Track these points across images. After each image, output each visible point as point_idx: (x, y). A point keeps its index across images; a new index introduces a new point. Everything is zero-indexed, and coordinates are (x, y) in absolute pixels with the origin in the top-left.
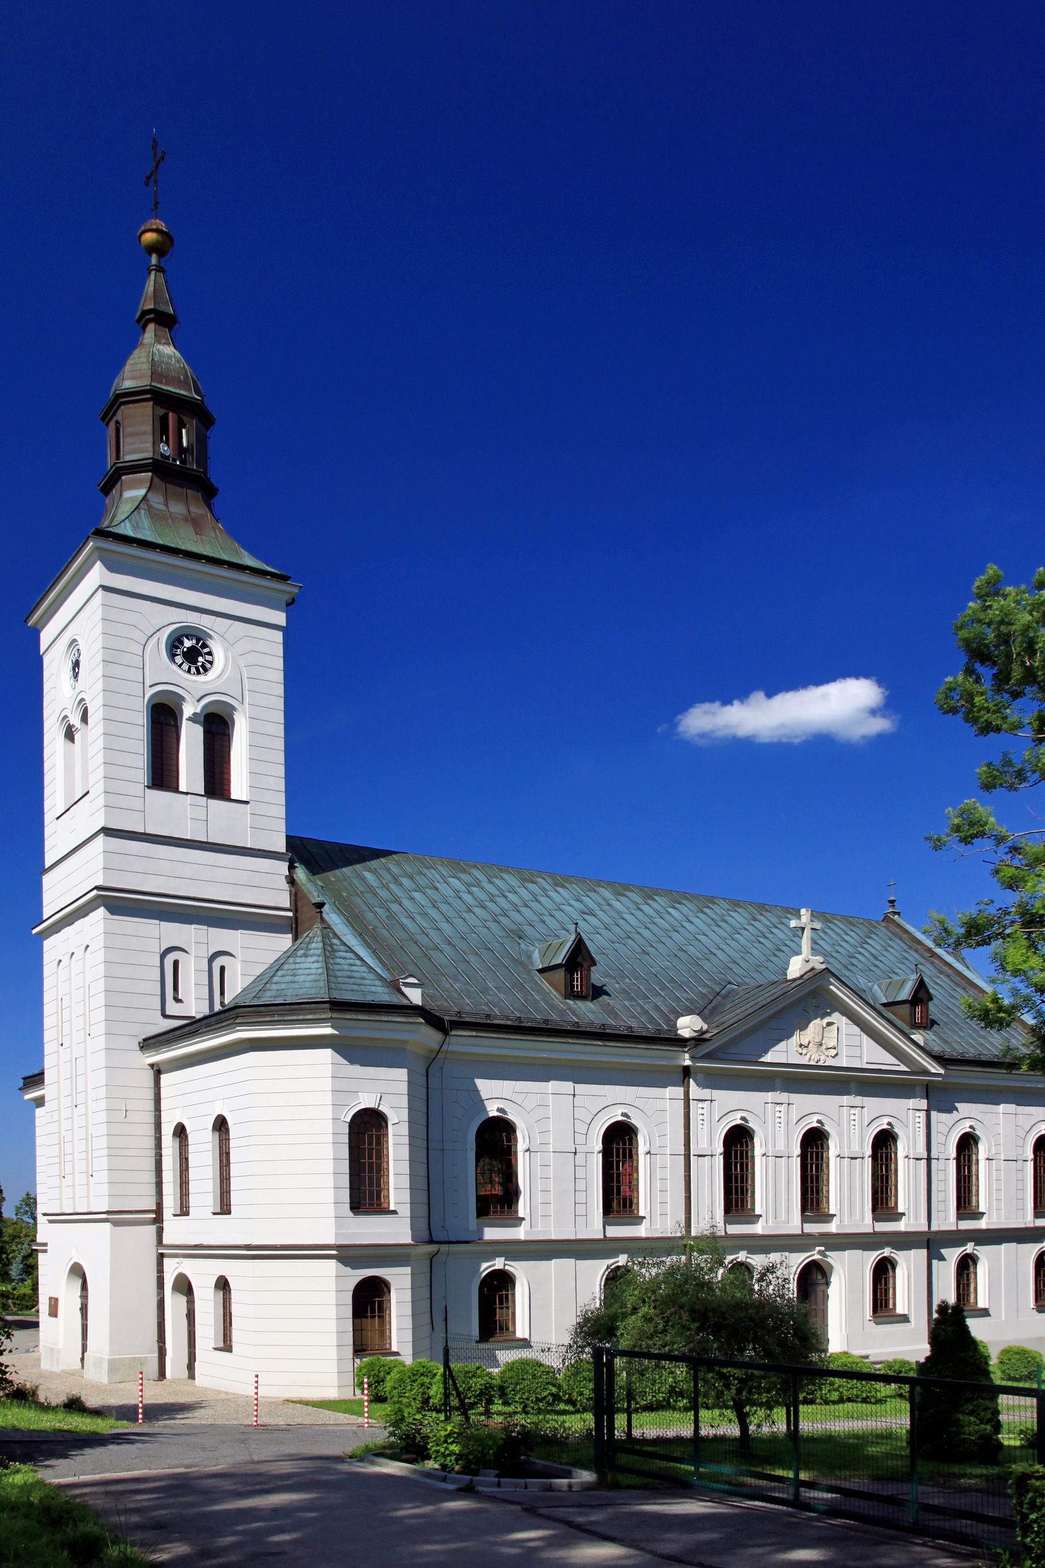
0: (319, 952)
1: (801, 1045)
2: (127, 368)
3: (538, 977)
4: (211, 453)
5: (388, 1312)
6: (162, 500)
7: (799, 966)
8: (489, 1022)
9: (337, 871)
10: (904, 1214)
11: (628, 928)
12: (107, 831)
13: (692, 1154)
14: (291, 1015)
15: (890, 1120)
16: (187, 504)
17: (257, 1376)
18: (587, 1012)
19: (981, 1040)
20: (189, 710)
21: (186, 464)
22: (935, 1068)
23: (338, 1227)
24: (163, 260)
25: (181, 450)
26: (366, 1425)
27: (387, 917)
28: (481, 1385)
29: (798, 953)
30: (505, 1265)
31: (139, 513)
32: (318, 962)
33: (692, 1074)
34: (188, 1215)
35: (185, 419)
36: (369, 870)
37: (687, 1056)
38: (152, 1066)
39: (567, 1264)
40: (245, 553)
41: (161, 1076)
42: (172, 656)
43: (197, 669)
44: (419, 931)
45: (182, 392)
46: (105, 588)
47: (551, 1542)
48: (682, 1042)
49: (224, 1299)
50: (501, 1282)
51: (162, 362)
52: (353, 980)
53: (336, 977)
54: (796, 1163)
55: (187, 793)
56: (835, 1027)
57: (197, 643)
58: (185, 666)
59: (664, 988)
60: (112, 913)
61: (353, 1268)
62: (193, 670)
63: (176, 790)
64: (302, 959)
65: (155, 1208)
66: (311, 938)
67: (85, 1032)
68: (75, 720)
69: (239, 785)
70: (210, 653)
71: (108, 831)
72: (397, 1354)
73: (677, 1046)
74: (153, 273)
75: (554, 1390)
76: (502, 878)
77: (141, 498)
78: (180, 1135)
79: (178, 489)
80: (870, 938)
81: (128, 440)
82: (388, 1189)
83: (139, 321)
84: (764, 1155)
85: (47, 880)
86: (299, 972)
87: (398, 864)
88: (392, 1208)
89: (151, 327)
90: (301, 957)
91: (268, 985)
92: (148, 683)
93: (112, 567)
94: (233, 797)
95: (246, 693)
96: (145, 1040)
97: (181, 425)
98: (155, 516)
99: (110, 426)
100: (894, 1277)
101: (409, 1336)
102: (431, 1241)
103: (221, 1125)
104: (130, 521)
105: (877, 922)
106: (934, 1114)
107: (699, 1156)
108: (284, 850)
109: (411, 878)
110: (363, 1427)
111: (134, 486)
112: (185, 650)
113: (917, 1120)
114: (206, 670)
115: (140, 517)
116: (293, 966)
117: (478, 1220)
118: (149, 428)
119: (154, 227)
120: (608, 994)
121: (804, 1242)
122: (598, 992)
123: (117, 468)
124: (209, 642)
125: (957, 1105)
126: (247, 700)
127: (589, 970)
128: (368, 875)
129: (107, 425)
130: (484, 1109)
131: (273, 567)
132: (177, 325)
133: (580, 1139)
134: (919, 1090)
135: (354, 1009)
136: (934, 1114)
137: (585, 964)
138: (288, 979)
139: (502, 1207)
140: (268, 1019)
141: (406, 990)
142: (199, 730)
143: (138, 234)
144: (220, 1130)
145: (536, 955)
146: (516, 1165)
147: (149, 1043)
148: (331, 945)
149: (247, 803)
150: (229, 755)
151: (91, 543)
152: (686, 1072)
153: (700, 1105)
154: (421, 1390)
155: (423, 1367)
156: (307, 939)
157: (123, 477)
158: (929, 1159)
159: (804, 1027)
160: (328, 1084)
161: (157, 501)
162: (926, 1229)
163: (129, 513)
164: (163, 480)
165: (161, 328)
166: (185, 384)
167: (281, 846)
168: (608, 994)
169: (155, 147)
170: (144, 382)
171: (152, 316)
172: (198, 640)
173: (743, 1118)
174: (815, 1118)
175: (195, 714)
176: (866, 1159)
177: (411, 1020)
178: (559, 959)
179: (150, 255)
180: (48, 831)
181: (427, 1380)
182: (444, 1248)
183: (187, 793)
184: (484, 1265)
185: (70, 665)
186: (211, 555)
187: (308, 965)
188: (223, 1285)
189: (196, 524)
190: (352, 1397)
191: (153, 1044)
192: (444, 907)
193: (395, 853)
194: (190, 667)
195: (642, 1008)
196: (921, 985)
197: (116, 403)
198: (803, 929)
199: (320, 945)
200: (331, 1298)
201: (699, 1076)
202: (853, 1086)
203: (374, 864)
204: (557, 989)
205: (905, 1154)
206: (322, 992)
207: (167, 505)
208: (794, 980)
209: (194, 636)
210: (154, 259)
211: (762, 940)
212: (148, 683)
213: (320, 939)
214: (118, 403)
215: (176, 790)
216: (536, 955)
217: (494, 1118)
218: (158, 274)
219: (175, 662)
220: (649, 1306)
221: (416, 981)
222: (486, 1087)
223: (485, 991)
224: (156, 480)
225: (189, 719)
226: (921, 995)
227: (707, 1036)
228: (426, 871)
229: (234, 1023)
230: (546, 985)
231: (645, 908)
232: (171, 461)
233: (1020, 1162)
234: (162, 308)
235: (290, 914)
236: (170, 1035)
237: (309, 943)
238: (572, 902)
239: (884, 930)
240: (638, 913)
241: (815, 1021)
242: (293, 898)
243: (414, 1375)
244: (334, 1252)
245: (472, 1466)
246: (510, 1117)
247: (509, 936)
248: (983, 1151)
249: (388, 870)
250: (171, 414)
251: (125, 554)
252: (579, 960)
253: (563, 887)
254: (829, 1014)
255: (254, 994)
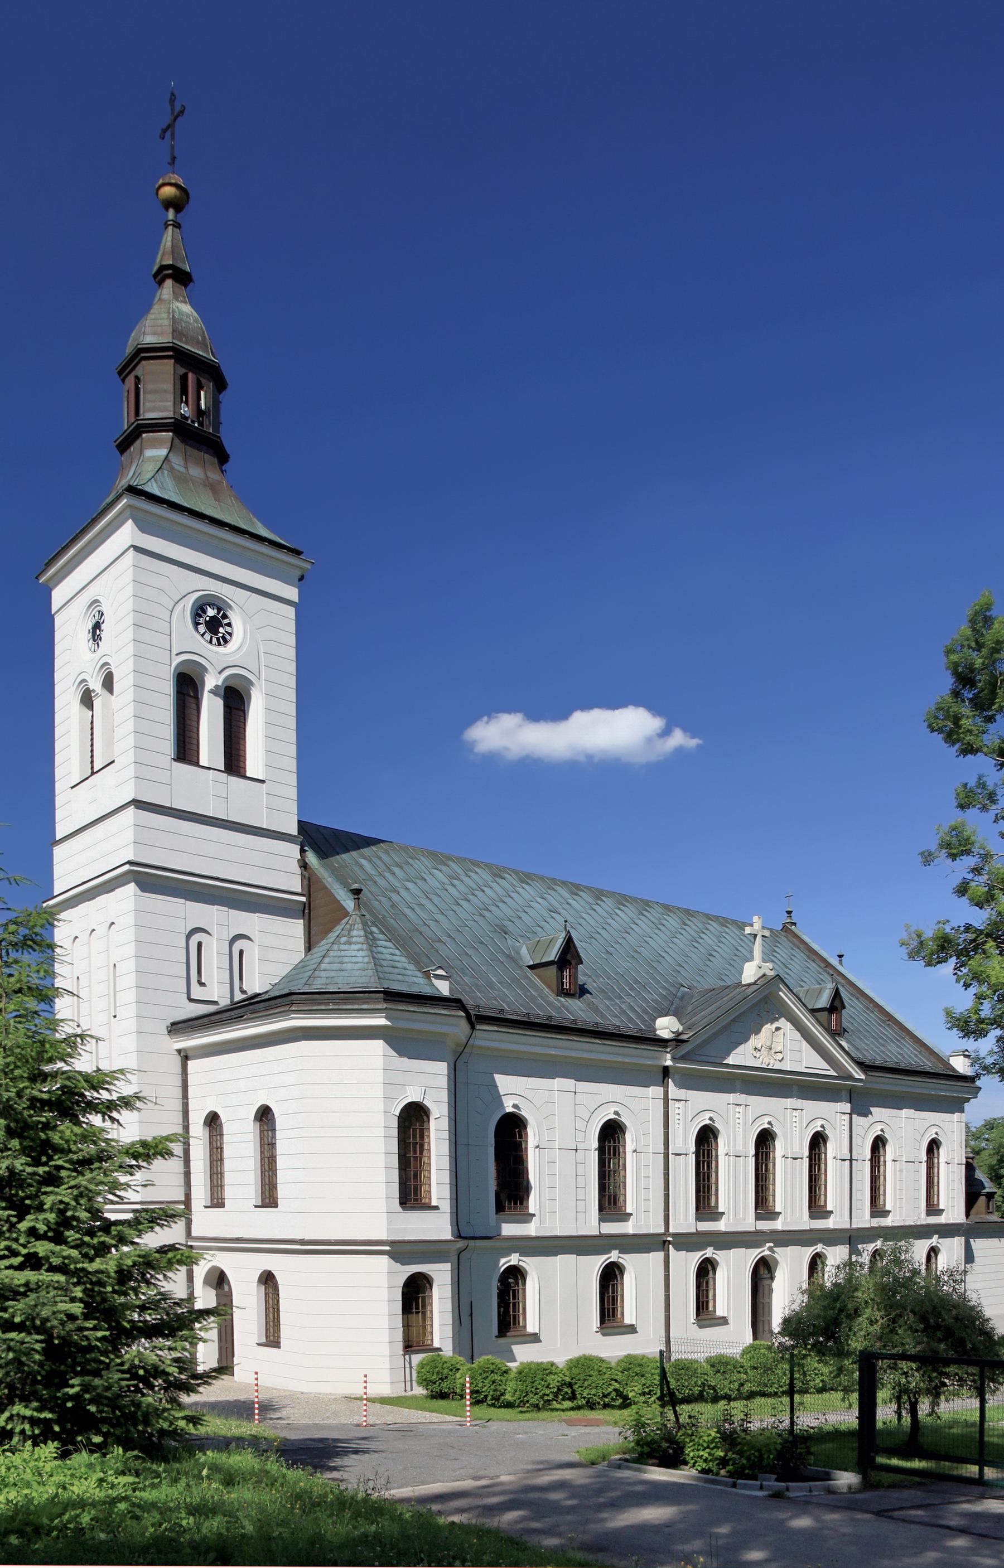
0: (361, 940)
1: (756, 1049)
2: (148, 323)
3: (529, 973)
4: (222, 419)
5: (429, 1308)
6: (182, 463)
7: (753, 972)
8: (502, 1016)
9: (337, 857)
10: (832, 1212)
11: (589, 928)
12: (138, 804)
13: (670, 1152)
14: (345, 1004)
15: (712, 1115)
16: (204, 468)
17: (366, 1376)
18: (575, 1010)
19: (882, 1048)
20: (211, 681)
21: (203, 427)
22: (858, 1074)
23: (390, 1222)
24: (179, 215)
25: (200, 413)
26: (468, 1424)
27: (391, 906)
28: (558, 1381)
29: (751, 959)
30: (519, 1260)
31: (163, 473)
32: (362, 950)
33: (671, 1075)
34: (224, 1207)
35: (203, 380)
36: (365, 858)
37: (669, 1056)
38: (179, 1051)
39: (571, 1258)
40: (260, 524)
41: (189, 1062)
42: (196, 624)
43: (218, 639)
44: (421, 923)
45: (200, 353)
46: (137, 549)
47: (973, 1551)
48: (663, 1042)
49: (266, 1294)
50: (516, 1274)
51: (182, 320)
52: (396, 971)
53: (382, 966)
54: (752, 1161)
55: (209, 768)
56: (781, 1032)
57: (218, 613)
58: (208, 636)
59: (632, 989)
60: (143, 890)
61: (403, 1264)
62: (214, 640)
63: (196, 764)
64: (346, 947)
65: (183, 1199)
66: (351, 926)
67: (110, 1013)
68: (96, 684)
69: (254, 762)
70: (229, 625)
71: (138, 804)
72: (439, 1349)
73: (660, 1046)
74: (170, 228)
75: (617, 1385)
76: (476, 873)
77: (163, 458)
78: (210, 1125)
79: (196, 452)
80: (776, 946)
81: (149, 397)
82: (430, 1185)
83: (155, 276)
84: (727, 1155)
85: (59, 852)
86: (346, 959)
87: (386, 852)
88: (434, 1203)
89: (169, 283)
90: (344, 944)
91: (317, 972)
92: (174, 652)
93: (144, 527)
94: (248, 775)
95: (263, 668)
96: (173, 1024)
97: (199, 387)
98: (180, 480)
99: (127, 381)
100: (524, 1290)
101: (449, 1332)
102: (460, 1237)
103: (265, 1115)
104: (155, 480)
105: (777, 931)
106: (854, 1116)
107: (677, 1155)
108: (296, 834)
109: (401, 867)
110: (466, 1425)
111: (154, 445)
112: (208, 619)
113: (737, 1115)
114: (226, 641)
115: (164, 477)
116: (338, 954)
117: (498, 1216)
118: (169, 386)
119: (173, 181)
120: (591, 994)
121: (758, 1238)
122: (583, 991)
123: (138, 424)
124: (229, 613)
125: (872, 1109)
126: (263, 676)
127: (577, 968)
128: (364, 862)
129: (123, 381)
130: (501, 1104)
131: (281, 539)
132: (192, 284)
133: (580, 1136)
134: (845, 1094)
135: (404, 999)
136: (854, 1116)
137: (573, 962)
138: (336, 966)
139: (515, 1203)
140: (323, 1007)
141: (437, 982)
142: (220, 703)
143: (157, 186)
144: (261, 1120)
145: (524, 950)
146: (527, 1161)
147: (177, 1028)
148: (372, 933)
149: (263, 782)
150: (245, 731)
151: (125, 500)
152: (666, 1071)
153: (677, 1104)
154: (492, 1387)
155: (493, 1364)
156: (348, 926)
157: (144, 435)
158: (851, 1160)
159: (757, 1032)
160: (379, 1076)
161: (177, 462)
162: (848, 1226)
163: (154, 472)
164: (182, 441)
165: (178, 285)
166: (203, 345)
167: (295, 832)
168: (591, 994)
169: (172, 100)
170: (165, 339)
171: (170, 272)
172: (219, 610)
173: (711, 1119)
174: (767, 1119)
175: (217, 686)
176: (804, 1159)
177: (453, 1013)
178: (552, 955)
179: (167, 209)
180: (59, 801)
181: (496, 1377)
182: (471, 1243)
183: (209, 768)
184: (503, 1261)
185: (90, 625)
186: (232, 523)
187: (354, 953)
188: (268, 1279)
189: (214, 489)
190: (403, 1394)
191: (184, 1029)
192: (435, 899)
193: (383, 841)
194: (211, 637)
195: (620, 1008)
196: (837, 994)
197: (136, 357)
198: (755, 936)
199: (362, 933)
200: (384, 1294)
201: (677, 1076)
202: (738, 1083)
203: (367, 851)
204: (549, 987)
205: (783, 1154)
206: (372, 980)
207: (186, 468)
208: (749, 985)
209: (214, 605)
210: (171, 214)
211: (696, 945)
212: (174, 652)
213: (360, 926)
214: (139, 358)
215: (196, 764)
216: (524, 950)
217: (509, 1113)
218: (175, 229)
219: (198, 631)
220: (873, 1308)
221: (444, 973)
222: (505, 1083)
223: (491, 985)
224: (177, 441)
225: (211, 691)
226: (836, 1005)
227: (684, 1037)
228: (410, 861)
229: (289, 1011)
230: (538, 982)
231: (596, 907)
232: (189, 422)
233: (917, 1163)
234: (179, 265)
235: (303, 899)
236: (205, 1020)
237: (350, 930)
238: (539, 900)
239: (783, 938)
240: (591, 912)
241: (766, 1026)
242: (306, 882)
243: (485, 1372)
244: (387, 1248)
245: (747, 1471)
246: (524, 1113)
247: (496, 931)
248: (890, 1152)
249: (380, 858)
250: (190, 375)
251: (151, 513)
252: (569, 957)
253: (527, 883)
254: (777, 1019)
255: (304, 981)
